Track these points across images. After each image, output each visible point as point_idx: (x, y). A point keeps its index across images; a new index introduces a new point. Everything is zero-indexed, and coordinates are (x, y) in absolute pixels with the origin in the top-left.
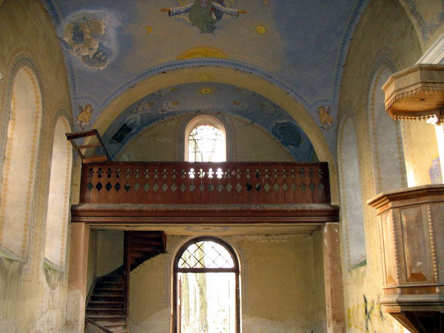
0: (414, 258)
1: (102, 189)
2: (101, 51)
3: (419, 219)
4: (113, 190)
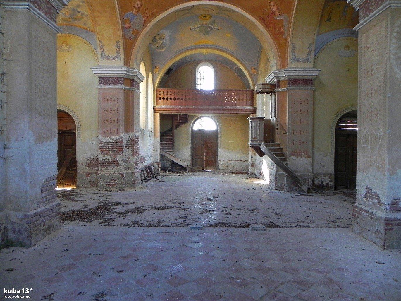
0: (82, 174)
4: (169, 100)
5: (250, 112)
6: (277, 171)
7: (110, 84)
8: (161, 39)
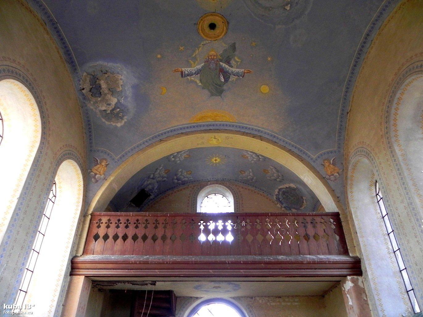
1: (108, 240)
2: (118, 108)
4: (120, 240)
5: (344, 272)
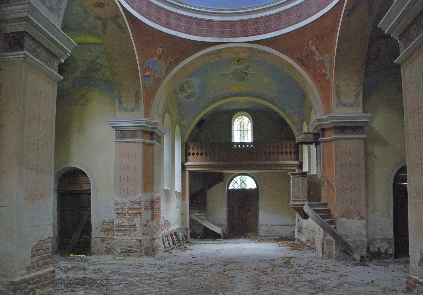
1: (194, 156)
3: (299, 180)
6: (325, 236)
7: (127, 138)
8: (189, 88)
